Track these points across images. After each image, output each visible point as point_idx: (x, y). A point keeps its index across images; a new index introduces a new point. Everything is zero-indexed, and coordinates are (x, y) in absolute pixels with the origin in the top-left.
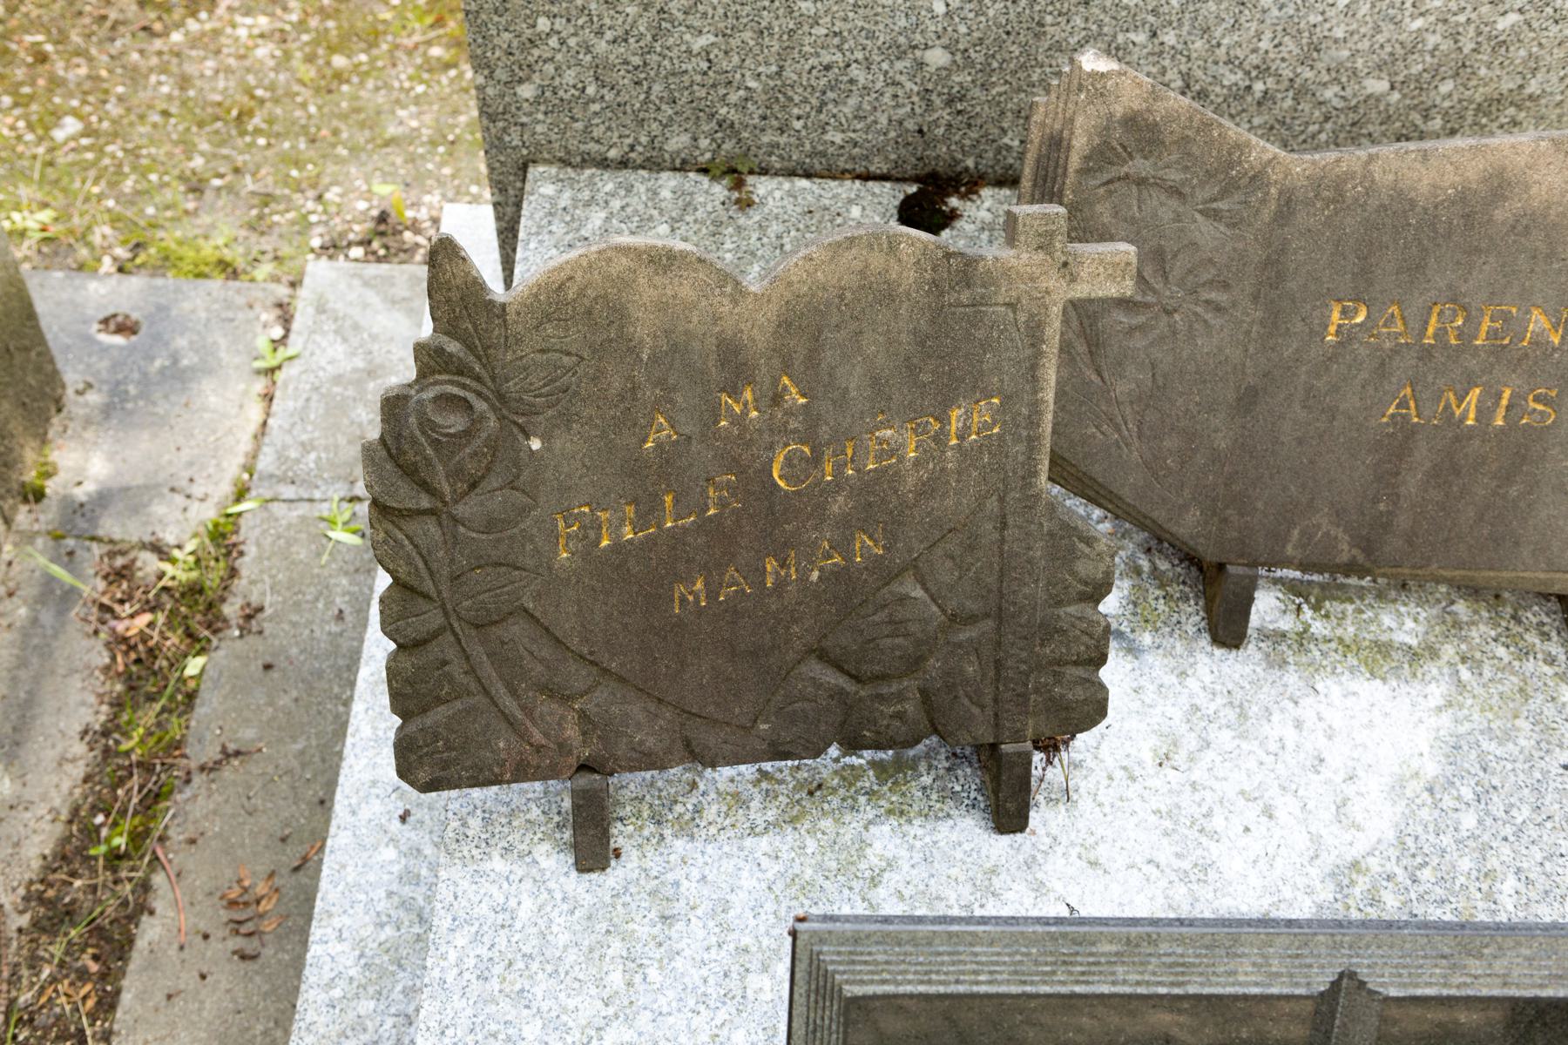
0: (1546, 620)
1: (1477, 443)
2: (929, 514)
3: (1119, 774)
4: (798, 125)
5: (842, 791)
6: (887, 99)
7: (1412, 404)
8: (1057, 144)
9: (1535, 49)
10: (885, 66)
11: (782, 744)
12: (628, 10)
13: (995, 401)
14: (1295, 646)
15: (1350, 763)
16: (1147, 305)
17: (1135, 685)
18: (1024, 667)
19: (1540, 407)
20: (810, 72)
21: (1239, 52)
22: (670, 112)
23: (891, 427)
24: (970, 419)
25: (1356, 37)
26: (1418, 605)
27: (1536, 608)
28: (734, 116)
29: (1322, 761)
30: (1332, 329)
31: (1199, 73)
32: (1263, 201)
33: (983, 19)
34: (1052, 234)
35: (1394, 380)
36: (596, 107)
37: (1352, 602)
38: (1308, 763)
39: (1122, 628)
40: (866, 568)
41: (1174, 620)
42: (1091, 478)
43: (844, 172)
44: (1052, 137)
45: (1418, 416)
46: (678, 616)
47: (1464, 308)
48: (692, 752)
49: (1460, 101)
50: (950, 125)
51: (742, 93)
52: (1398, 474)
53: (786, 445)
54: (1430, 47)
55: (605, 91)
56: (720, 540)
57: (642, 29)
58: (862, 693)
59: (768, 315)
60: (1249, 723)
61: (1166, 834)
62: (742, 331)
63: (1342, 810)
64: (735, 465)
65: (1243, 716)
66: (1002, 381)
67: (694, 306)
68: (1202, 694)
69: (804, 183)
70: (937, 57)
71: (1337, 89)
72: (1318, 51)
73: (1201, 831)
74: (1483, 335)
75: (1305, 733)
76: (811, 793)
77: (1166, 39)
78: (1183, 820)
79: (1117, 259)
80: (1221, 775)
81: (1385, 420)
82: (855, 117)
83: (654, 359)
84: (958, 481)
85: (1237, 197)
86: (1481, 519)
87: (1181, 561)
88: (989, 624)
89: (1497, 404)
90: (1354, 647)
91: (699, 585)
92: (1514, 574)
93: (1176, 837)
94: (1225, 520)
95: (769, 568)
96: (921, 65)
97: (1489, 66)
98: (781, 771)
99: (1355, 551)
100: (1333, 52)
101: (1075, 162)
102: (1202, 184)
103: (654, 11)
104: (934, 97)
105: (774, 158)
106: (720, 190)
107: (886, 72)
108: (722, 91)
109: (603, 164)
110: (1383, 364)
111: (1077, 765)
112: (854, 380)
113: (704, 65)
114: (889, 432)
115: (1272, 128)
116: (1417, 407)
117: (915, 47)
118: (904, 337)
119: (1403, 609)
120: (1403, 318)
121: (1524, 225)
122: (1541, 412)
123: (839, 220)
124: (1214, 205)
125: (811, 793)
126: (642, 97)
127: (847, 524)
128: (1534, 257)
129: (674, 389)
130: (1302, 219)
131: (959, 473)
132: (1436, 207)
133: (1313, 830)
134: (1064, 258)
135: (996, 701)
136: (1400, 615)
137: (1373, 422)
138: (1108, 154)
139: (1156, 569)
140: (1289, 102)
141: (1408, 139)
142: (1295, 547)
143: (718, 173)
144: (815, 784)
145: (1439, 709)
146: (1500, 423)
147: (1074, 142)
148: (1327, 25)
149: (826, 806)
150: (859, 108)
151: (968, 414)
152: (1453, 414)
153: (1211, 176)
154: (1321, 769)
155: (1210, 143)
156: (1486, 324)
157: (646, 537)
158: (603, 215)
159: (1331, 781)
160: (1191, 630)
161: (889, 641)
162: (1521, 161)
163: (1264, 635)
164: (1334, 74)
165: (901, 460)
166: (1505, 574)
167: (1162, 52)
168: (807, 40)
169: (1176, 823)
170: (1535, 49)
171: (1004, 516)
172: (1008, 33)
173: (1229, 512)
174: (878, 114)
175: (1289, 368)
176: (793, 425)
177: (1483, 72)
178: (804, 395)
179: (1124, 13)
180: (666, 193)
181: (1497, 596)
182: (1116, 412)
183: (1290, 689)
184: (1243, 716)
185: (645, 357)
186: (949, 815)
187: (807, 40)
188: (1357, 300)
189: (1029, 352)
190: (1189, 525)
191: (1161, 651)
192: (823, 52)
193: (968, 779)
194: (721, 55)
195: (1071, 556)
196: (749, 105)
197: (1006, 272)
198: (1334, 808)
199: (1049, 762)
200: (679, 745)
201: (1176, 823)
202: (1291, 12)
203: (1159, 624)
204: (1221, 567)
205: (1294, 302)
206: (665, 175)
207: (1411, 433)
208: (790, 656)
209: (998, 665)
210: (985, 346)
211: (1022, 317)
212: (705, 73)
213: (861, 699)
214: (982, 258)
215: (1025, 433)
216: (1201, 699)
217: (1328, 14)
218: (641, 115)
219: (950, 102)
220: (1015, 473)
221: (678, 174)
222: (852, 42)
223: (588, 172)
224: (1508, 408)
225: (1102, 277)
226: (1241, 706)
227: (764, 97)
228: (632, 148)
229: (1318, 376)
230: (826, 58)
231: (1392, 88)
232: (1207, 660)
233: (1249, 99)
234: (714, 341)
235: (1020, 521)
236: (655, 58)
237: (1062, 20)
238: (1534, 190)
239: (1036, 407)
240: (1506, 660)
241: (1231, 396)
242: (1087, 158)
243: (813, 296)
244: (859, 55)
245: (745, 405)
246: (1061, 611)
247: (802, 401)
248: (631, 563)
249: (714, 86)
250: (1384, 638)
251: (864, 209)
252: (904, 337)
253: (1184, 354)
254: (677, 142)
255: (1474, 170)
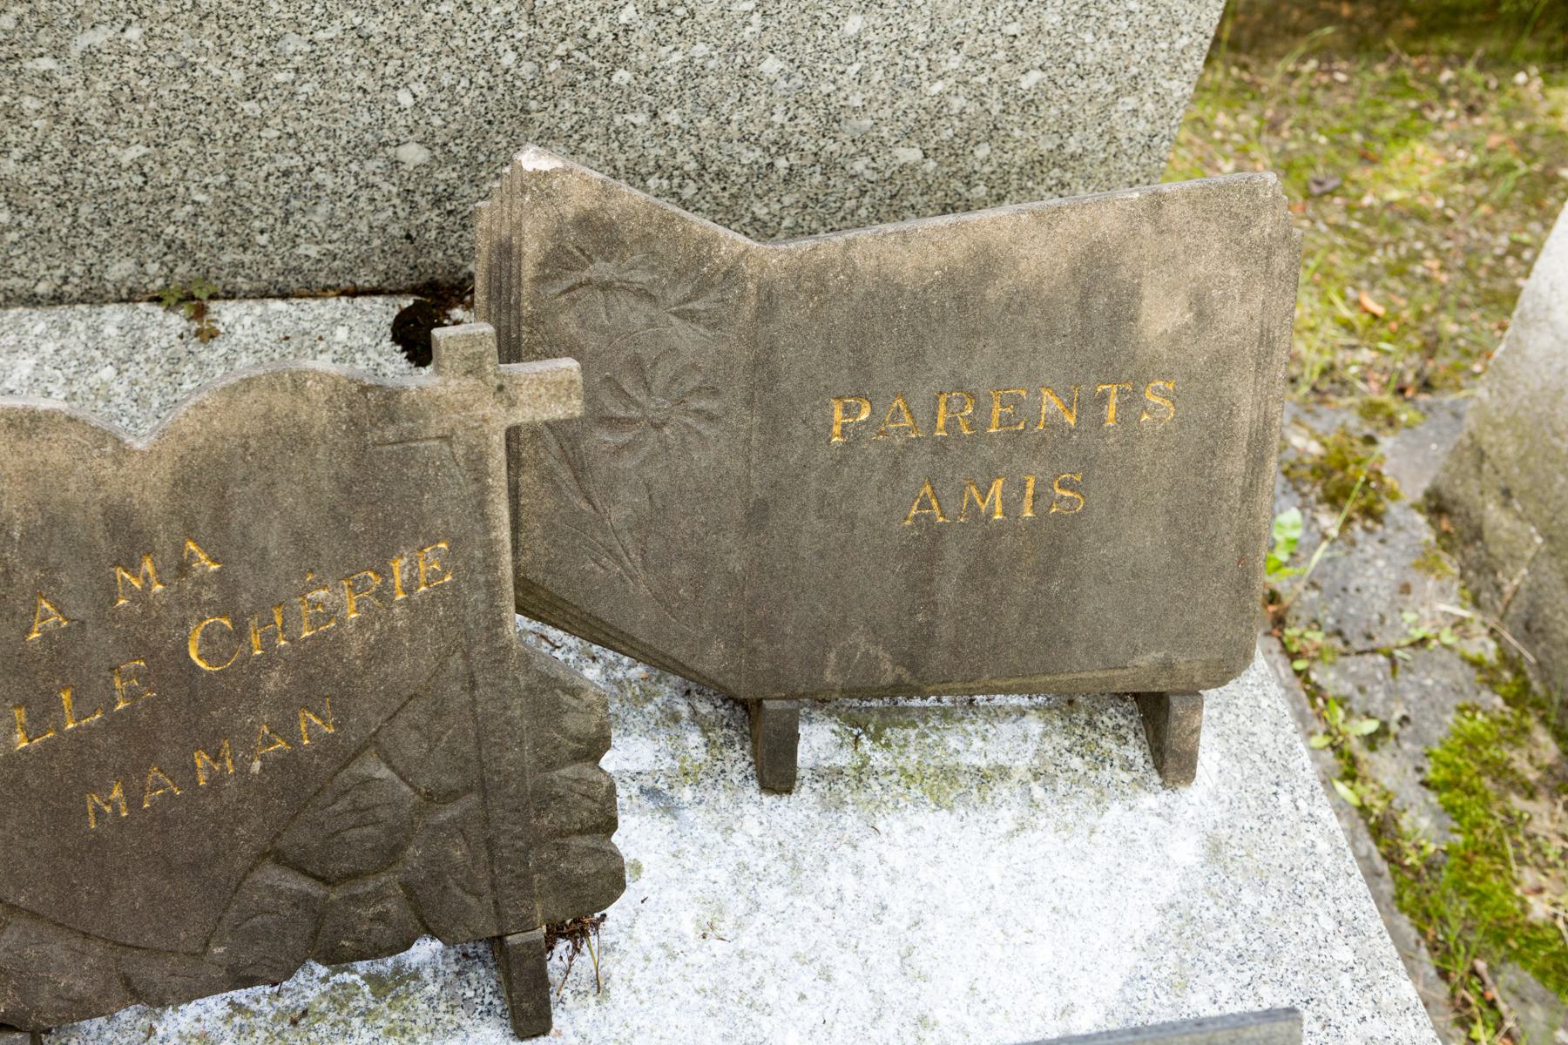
0: (1122, 722)
1: (1008, 538)
2: (383, 681)
3: (657, 953)
4: (263, 239)
5: (332, 1016)
6: (363, 203)
7: (934, 503)
8: (506, 252)
9: (1066, 107)
10: (354, 167)
11: (242, 969)
12: (36, 124)
13: (443, 545)
14: (853, 784)
15: (915, 907)
16: (632, 421)
17: (674, 849)
18: (520, 844)
19: (1068, 494)
20: (266, 179)
21: (752, 128)
22: (105, 235)
23: (325, 587)
24: (415, 569)
25: (875, 105)
26: (986, 721)
27: (1112, 710)
28: (183, 234)
29: (884, 908)
30: (837, 429)
31: (713, 153)
32: (742, 298)
33: (457, 108)
34: (481, 356)
35: (911, 478)
36: (13, 236)
37: (916, 727)
38: (869, 913)
39: (659, 786)
40: (317, 751)
41: (717, 769)
42: (597, 619)
43: (325, 289)
44: (501, 245)
45: (943, 515)
46: (94, 832)
47: (972, 396)
48: (133, 992)
49: (1000, 165)
50: (441, 228)
51: (189, 208)
52: (931, 580)
53: (202, 619)
54: (956, 111)
55: (22, 217)
56: (137, 738)
57: (56, 144)
58: (333, 897)
59: (163, 470)
60: (803, 877)
61: (712, 1014)
62: (131, 495)
63: (907, 961)
64: (142, 648)
65: (796, 869)
66: (447, 523)
67: (70, 471)
68: (750, 850)
69: (279, 305)
70: (413, 154)
71: (867, 160)
72: (838, 122)
73: (750, 1006)
74: (995, 421)
75: (865, 880)
76: (294, 1023)
77: (669, 118)
78: (730, 996)
79: (558, 378)
80: (773, 938)
81: (908, 523)
82: (330, 226)
83: (29, 536)
84: (412, 640)
85: (714, 295)
86: (1027, 620)
87: (725, 701)
88: (474, 798)
89: (1023, 493)
90: (917, 777)
91: (117, 793)
92: (1071, 677)
93: (722, 1016)
94: (754, 651)
95: (199, 763)
96: (396, 163)
97: (1022, 127)
98: (258, 1001)
99: (899, 670)
100: (854, 122)
101: (529, 270)
102: (673, 284)
103: (68, 123)
104: (417, 198)
105: (239, 279)
106: (177, 321)
107: (356, 175)
108: (165, 208)
109: (33, 301)
110: (896, 463)
111: (609, 949)
112: (272, 537)
113: (139, 180)
114: (322, 593)
115: (805, 207)
116: (939, 505)
117: (385, 144)
118: (325, 484)
119: (970, 728)
120: (910, 411)
121: (1019, 302)
122: (1069, 499)
123: (322, 345)
124: (690, 306)
125: (294, 1023)
126: (68, 221)
127: (287, 705)
128: (1035, 336)
129: (57, 568)
130: (785, 313)
131: (412, 631)
132: (925, 291)
133: (874, 986)
134: (497, 382)
135: (493, 886)
136: (967, 734)
137: (896, 527)
138: (566, 259)
139: (696, 713)
140: (817, 179)
141: (954, 210)
142: (834, 673)
143: (173, 301)
144: (299, 1011)
145: (1011, 834)
146: (1029, 514)
147: (525, 249)
148: (842, 94)
149: (313, 1035)
150: (332, 216)
151: (413, 564)
152: (978, 509)
153: (681, 275)
154: (885, 918)
155: (674, 239)
156: (997, 410)
157: (44, 743)
158: (32, 361)
159: (894, 928)
160: (736, 778)
161: (356, 831)
162: (1005, 235)
163: (818, 774)
164: (860, 146)
165: (341, 622)
166: (1063, 678)
167: (667, 134)
168: (257, 144)
169: (723, 1000)
170: (1066, 107)
171: (472, 675)
172: (490, 123)
173: (756, 641)
174: (356, 221)
175: (797, 476)
176: (206, 595)
177: (1017, 133)
178: (215, 561)
179: (617, 94)
180: (110, 330)
181: (1071, 702)
182: (615, 542)
183: (848, 833)
184: (796, 869)
185: (16, 535)
186: (459, 1027)
187: (257, 144)
188: (858, 396)
189: (473, 488)
190: (714, 658)
191: (703, 807)
192: (278, 156)
193: (483, 982)
194: (157, 167)
195: (554, 712)
196: (200, 220)
197: (435, 402)
198: (897, 959)
199: (577, 950)
200: (117, 984)
201: (723, 1000)
202: (800, 83)
203: (700, 776)
204: (759, 702)
205: (791, 404)
206: (109, 309)
207: (937, 534)
208: (240, 864)
209: (490, 844)
210: (422, 485)
211: (460, 451)
212: (141, 189)
213: (333, 904)
214: (404, 389)
215: (482, 579)
216: (749, 857)
217: (840, 83)
218: (71, 241)
219: (437, 202)
220: (476, 623)
221: (125, 306)
222: (310, 143)
223: (13, 312)
224: (1035, 497)
225: (544, 399)
226: (794, 858)
227: (217, 211)
228: (65, 280)
229: (830, 482)
230: (284, 164)
231: (926, 156)
232: (754, 810)
233: (774, 177)
234: (98, 508)
235: (490, 677)
236: (77, 175)
237: (549, 104)
238: (1023, 266)
239: (490, 548)
240: (1081, 772)
241: (739, 512)
242: (542, 265)
243: (211, 447)
244: (322, 158)
245: (145, 579)
246: (555, 775)
247: (214, 567)
248: (29, 776)
249: (154, 202)
250: (950, 762)
251: (351, 329)
252: (325, 484)
253: (681, 471)
254: (120, 269)
255: (958, 249)
